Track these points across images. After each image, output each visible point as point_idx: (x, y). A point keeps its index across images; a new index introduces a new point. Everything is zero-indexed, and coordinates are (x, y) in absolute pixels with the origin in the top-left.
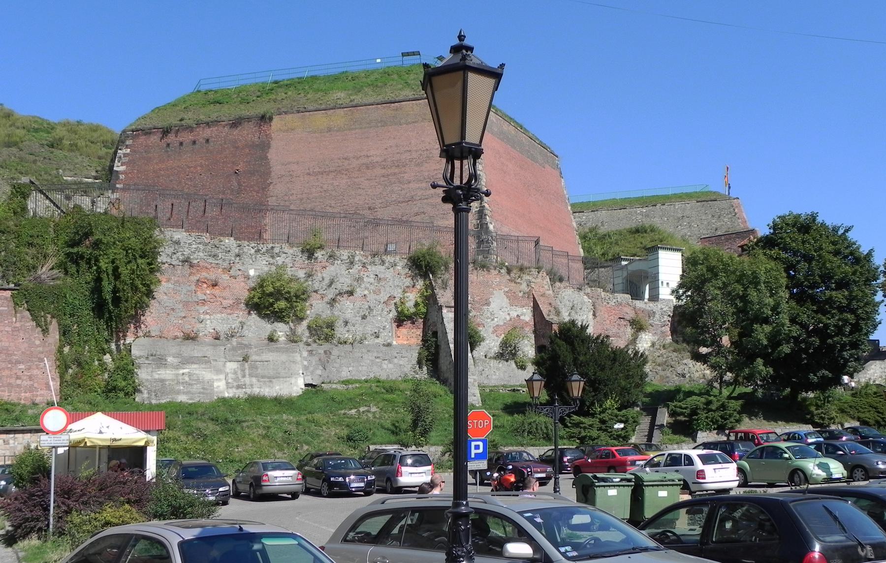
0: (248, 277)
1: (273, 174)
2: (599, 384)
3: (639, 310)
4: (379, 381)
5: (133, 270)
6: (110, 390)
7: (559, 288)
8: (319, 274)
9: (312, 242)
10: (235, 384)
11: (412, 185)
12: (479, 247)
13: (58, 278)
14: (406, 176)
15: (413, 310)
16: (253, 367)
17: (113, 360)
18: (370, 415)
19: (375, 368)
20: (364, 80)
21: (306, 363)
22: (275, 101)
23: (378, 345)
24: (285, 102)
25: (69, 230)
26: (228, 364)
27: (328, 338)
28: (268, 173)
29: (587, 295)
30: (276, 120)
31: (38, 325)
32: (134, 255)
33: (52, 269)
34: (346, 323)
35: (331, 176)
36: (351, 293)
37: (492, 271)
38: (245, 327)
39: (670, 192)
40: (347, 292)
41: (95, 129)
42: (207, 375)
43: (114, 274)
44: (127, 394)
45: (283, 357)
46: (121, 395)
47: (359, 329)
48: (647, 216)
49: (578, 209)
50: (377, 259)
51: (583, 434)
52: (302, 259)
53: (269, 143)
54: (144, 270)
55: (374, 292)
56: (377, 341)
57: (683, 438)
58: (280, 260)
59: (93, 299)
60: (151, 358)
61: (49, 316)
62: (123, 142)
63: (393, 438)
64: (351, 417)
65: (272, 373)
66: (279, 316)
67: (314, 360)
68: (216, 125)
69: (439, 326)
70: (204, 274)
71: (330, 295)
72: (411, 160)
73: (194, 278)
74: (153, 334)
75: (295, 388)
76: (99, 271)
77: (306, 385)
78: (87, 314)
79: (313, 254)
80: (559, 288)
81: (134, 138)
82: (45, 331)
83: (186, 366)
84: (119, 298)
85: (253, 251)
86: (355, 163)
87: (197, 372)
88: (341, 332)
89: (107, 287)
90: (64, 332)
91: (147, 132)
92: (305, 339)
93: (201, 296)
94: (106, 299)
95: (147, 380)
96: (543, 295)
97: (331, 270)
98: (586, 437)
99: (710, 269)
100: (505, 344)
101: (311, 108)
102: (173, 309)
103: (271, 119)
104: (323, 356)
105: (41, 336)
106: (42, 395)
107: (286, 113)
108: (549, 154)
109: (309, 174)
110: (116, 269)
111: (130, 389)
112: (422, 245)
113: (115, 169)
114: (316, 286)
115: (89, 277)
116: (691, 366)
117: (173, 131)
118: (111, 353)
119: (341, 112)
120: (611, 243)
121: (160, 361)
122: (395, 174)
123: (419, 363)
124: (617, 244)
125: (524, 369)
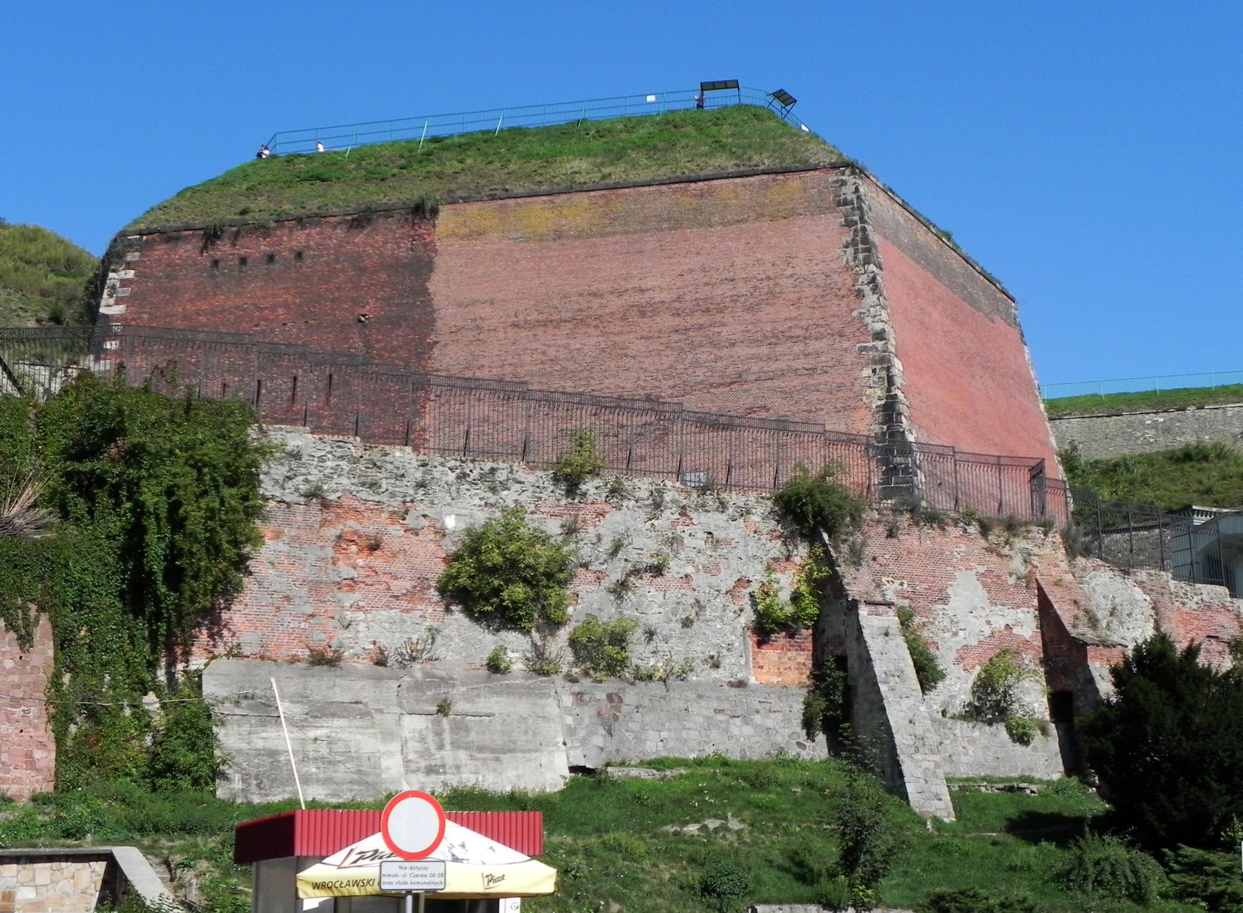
0: (442, 533)
1: (439, 324)
4: (725, 763)
5: (212, 510)
6: (160, 770)
7: (1084, 569)
8: (591, 529)
9: (577, 460)
10: (423, 764)
11: (741, 351)
12: (886, 481)
13: (45, 527)
14: (725, 332)
15: (790, 610)
16: (459, 727)
17: (163, 706)
19: (715, 735)
20: (624, 136)
21: (569, 720)
22: (440, 176)
23: (717, 685)
24: (461, 179)
27: (614, 667)
28: (428, 323)
29: (1141, 584)
30: (445, 213)
31: (11, 626)
32: (213, 479)
33: (34, 506)
35: (566, 329)
36: (657, 571)
37: (949, 529)
38: (439, 639)
39: (1212, 382)
41: (31, 236)
44: (196, 782)
45: (522, 707)
46: (185, 782)
47: (677, 648)
48: (1167, 430)
49: (1057, 410)
50: (709, 498)
51: (1213, 888)
52: (554, 495)
54: (234, 511)
55: (706, 569)
56: (715, 674)
58: (509, 497)
59: (124, 572)
60: (244, 703)
61: (33, 607)
62: (120, 256)
63: (804, 890)
64: (691, 840)
65: (499, 741)
67: (588, 713)
68: (318, 224)
70: (352, 524)
71: (616, 572)
74: (246, 650)
75: (548, 776)
76: (139, 510)
78: (109, 604)
79: (577, 485)
80: (1084, 569)
81: (143, 247)
82: (25, 640)
83: (320, 722)
84: (181, 570)
85: (452, 477)
86: (615, 303)
87: (345, 736)
88: (639, 654)
89: (155, 546)
90: (63, 642)
91: (171, 237)
92: (565, 669)
93: (346, 571)
94: (151, 573)
95: (240, 751)
96: (1058, 583)
100: (985, 685)
101: (519, 190)
102: (288, 598)
103: (435, 212)
104: (605, 706)
105: (17, 649)
106: (15, 781)
107: (466, 200)
108: (1000, 295)
109: (515, 325)
110: (174, 507)
111: (205, 771)
112: (805, 471)
113: (102, 310)
114: (586, 552)
115: (115, 525)
117: (226, 235)
118: (157, 690)
119: (582, 199)
120: (1132, 483)
121: (265, 711)
122: (701, 327)
123: (808, 724)
124: (1144, 482)
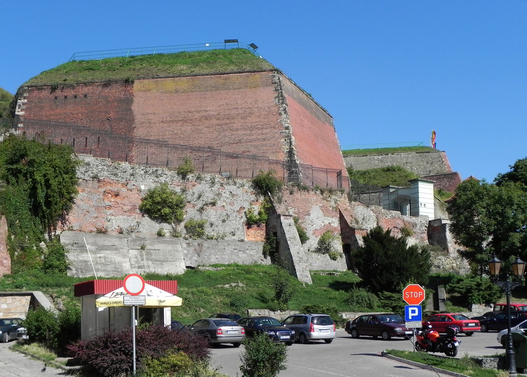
0: (140, 191)
1: (136, 121)
2: (404, 270)
3: (407, 222)
5: (60, 182)
6: (47, 267)
7: (354, 206)
8: (191, 190)
10: (137, 265)
11: (239, 132)
12: (290, 176)
14: (235, 126)
15: (258, 217)
17: (47, 246)
18: (240, 289)
20: (198, 58)
21: (185, 252)
22: (134, 70)
24: (142, 71)
25: (7, 152)
26: (131, 251)
27: (200, 235)
28: (132, 120)
29: (373, 210)
32: (60, 172)
34: (212, 225)
35: (180, 123)
36: (214, 204)
37: (311, 192)
38: (140, 225)
40: (211, 203)
42: (116, 258)
43: (46, 185)
44: (60, 271)
45: (169, 247)
46: (57, 271)
47: (220, 229)
48: (382, 161)
49: (346, 154)
51: (394, 304)
52: (178, 179)
53: (132, 99)
55: (230, 204)
56: (233, 238)
57: (461, 308)
58: (162, 179)
60: (75, 245)
62: (22, 94)
64: (227, 290)
65: (162, 258)
66: (164, 219)
67: (191, 250)
69: (278, 229)
70: (109, 187)
71: (200, 205)
72: (238, 115)
73: (102, 190)
74: (75, 228)
75: (179, 269)
76: (34, 181)
77: (187, 267)
78: (26, 213)
79: (186, 176)
80: (354, 206)
81: (29, 92)
83: (101, 252)
84: (51, 202)
85: (142, 172)
86: (197, 115)
87: (110, 256)
88: (208, 231)
89: (41, 194)
91: (39, 88)
93: (108, 203)
94: (40, 203)
95: (74, 261)
96: (346, 210)
97: (199, 188)
98: (397, 306)
99: (477, 194)
100: (322, 242)
101: (163, 76)
102: (88, 212)
103: (133, 82)
104: (197, 248)
107: (144, 78)
108: (327, 115)
109: (163, 122)
110: (47, 181)
111: (63, 267)
113: (16, 113)
114: (189, 198)
115: (26, 186)
116: (444, 260)
117: (59, 88)
118: (45, 241)
119: (185, 79)
121: (82, 248)
122: (226, 124)
123: (264, 253)
124: (374, 178)
125: (335, 260)
